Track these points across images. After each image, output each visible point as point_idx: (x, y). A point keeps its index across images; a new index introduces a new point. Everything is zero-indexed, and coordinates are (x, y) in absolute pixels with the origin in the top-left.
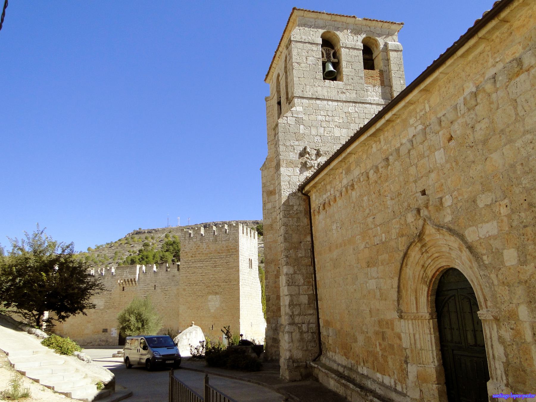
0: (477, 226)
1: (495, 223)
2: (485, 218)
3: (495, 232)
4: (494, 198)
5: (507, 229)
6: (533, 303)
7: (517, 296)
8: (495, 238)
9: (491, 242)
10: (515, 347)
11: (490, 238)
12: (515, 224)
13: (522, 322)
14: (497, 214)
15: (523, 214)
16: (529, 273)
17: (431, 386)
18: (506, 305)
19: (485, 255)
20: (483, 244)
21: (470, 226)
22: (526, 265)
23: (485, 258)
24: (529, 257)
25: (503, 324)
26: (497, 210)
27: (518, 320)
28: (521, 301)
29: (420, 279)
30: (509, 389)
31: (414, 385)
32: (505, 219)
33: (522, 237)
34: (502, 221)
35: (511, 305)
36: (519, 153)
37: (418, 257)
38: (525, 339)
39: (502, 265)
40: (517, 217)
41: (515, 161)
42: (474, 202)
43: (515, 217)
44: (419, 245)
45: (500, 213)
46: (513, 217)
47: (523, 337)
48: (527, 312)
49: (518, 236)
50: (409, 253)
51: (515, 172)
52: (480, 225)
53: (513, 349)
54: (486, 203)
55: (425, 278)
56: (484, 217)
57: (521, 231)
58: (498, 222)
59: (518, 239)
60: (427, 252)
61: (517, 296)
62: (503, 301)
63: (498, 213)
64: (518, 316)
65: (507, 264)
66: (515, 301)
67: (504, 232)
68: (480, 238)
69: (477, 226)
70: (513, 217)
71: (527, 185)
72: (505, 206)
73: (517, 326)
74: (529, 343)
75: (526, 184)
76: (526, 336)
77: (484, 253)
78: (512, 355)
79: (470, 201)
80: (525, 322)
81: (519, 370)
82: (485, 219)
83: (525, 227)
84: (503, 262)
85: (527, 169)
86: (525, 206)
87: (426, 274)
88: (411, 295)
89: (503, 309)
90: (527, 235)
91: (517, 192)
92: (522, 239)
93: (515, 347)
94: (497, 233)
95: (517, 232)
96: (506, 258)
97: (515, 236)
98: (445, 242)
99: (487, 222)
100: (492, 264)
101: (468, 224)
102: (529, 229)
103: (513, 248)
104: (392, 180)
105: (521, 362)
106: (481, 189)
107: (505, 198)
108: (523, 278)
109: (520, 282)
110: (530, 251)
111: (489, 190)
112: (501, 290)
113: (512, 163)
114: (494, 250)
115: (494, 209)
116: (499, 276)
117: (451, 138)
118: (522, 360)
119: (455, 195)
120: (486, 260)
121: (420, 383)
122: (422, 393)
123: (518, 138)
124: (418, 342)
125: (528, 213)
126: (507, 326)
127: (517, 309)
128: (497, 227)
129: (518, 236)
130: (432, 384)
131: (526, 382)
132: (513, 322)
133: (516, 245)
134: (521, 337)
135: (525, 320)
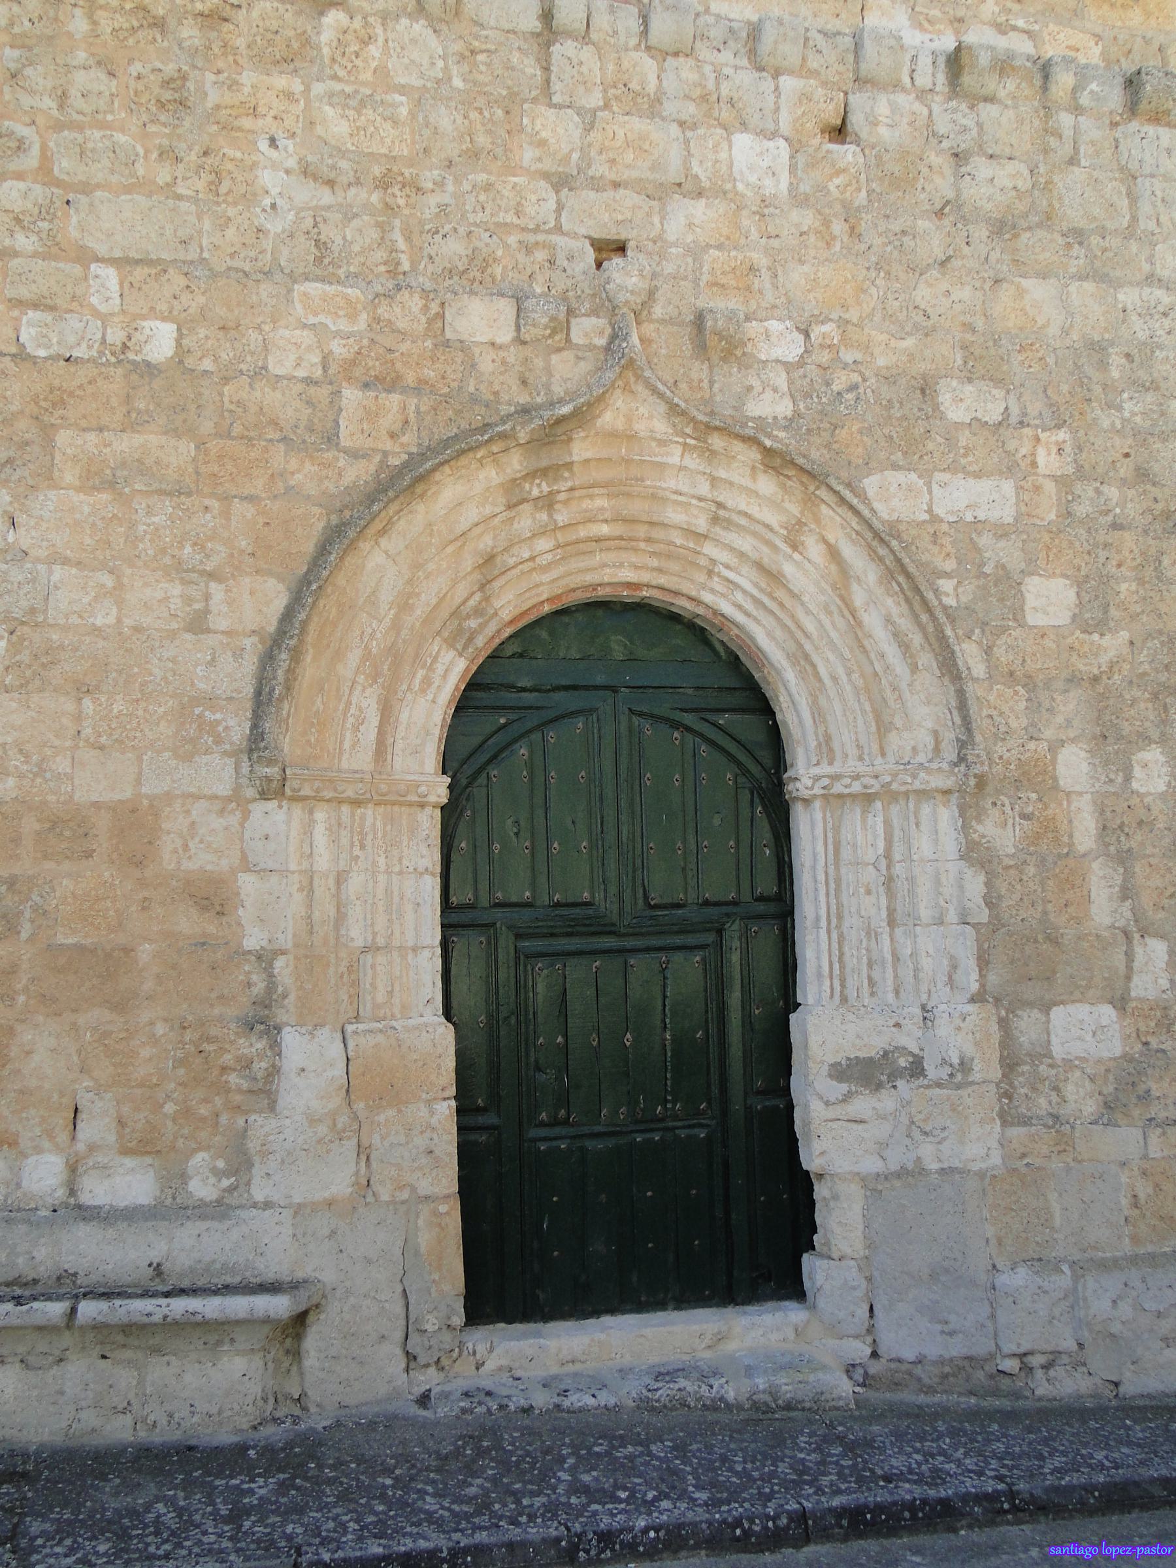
0: (927, 476)
1: (1008, 487)
2: (970, 459)
3: (1006, 514)
4: (1015, 410)
5: (1053, 516)
6: (1110, 740)
7: (1060, 719)
8: (1001, 532)
9: (985, 540)
10: (1031, 870)
11: (980, 526)
12: (1081, 510)
13: (1068, 794)
14: (1023, 465)
15: (1112, 492)
16: (1104, 659)
17: (423, 1112)
18: (1012, 742)
19: (947, 575)
20: (946, 541)
21: (895, 467)
22: (1102, 635)
23: (946, 585)
24: (1114, 612)
25: (994, 804)
26: (1023, 451)
27: (1055, 787)
28: (1072, 735)
29: (444, 613)
30: (989, 1006)
31: (322, 1130)
32: (1050, 487)
33: (1102, 555)
34: (1037, 489)
35: (1032, 745)
36: (1124, 321)
37: (471, 514)
38: (1071, 845)
39: (1015, 619)
40: (1091, 493)
41: (1107, 336)
42: (923, 391)
43: (1087, 491)
44: (515, 463)
45: (1034, 464)
46: (1078, 488)
47: (1066, 839)
48: (1085, 767)
49: (1086, 547)
50: (438, 476)
51: (1103, 365)
52: (939, 476)
53: (1025, 878)
54: (979, 415)
55: (468, 617)
56: (965, 455)
57: (1101, 537)
58: (1019, 489)
59: (1086, 557)
60: (548, 502)
61: (1060, 719)
62: (1003, 729)
63: (1028, 460)
64: (1055, 779)
65: (1032, 619)
66: (1048, 733)
67: (1038, 522)
68: (935, 519)
69: (927, 476)
70: (1078, 488)
71: (1138, 419)
72: (1054, 450)
73: (1046, 807)
74: (1084, 855)
75: (1133, 414)
76: (1076, 834)
77: (948, 568)
78: (1016, 897)
79: (903, 381)
80: (1080, 794)
81: (1036, 941)
82: (970, 463)
83: (1115, 526)
84: (1018, 614)
85: (1142, 375)
86: (1125, 469)
87: (487, 599)
88: (354, 682)
89: (1001, 758)
90: (1118, 552)
91: (1106, 424)
92: (1102, 560)
93: (1031, 870)
94: (1011, 520)
95: (1085, 535)
96: (1031, 601)
97: (1077, 544)
98: (704, 489)
99: (978, 475)
100: (974, 611)
101: (883, 455)
102: (1128, 539)
103: (1067, 577)
104: (338, 86)
105: (1045, 913)
106: (959, 362)
107: (1058, 427)
108: (1082, 668)
109: (1073, 680)
110: (1122, 596)
111: (998, 382)
112: (999, 696)
113: (1096, 338)
114: (987, 569)
115: (1011, 445)
116: (999, 651)
117: (840, 132)
118: (1050, 907)
119: (824, 336)
120: (948, 595)
121: (362, 1115)
122: (363, 1164)
123: (1131, 284)
124: (355, 912)
125: (1131, 493)
126: (1008, 809)
127: (1054, 762)
128: (1014, 500)
129: (1086, 547)
130: (429, 1102)
131: (1054, 972)
132: (1034, 796)
133: (1079, 570)
134: (1057, 840)
135: (1078, 788)
